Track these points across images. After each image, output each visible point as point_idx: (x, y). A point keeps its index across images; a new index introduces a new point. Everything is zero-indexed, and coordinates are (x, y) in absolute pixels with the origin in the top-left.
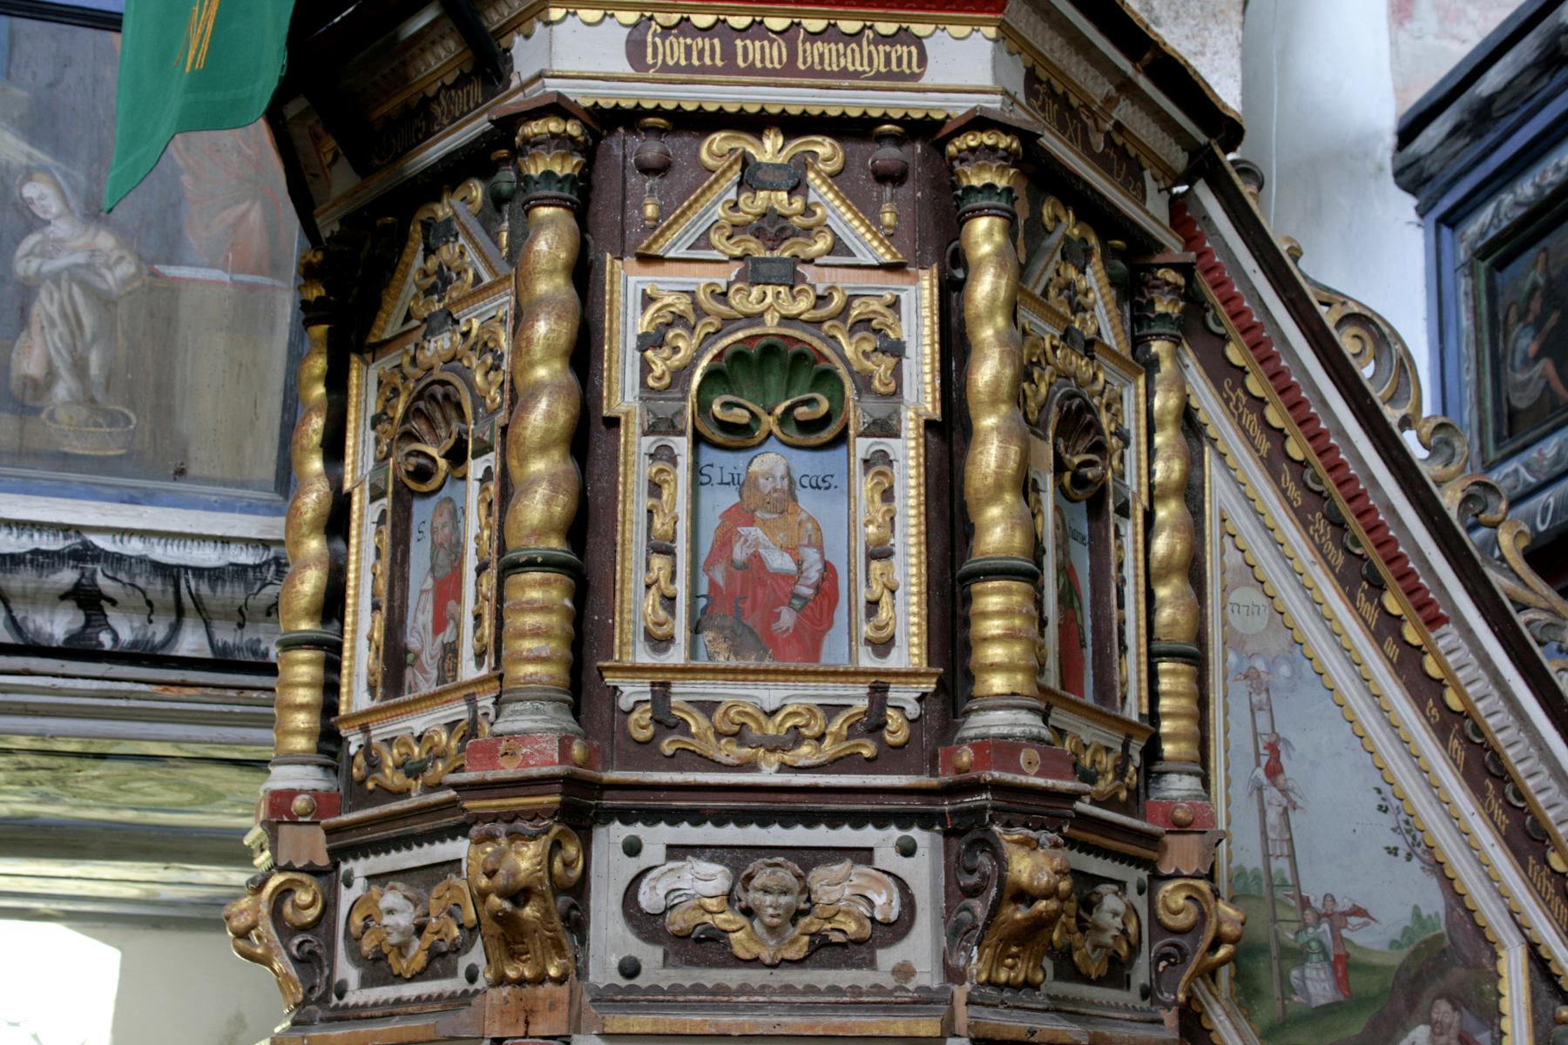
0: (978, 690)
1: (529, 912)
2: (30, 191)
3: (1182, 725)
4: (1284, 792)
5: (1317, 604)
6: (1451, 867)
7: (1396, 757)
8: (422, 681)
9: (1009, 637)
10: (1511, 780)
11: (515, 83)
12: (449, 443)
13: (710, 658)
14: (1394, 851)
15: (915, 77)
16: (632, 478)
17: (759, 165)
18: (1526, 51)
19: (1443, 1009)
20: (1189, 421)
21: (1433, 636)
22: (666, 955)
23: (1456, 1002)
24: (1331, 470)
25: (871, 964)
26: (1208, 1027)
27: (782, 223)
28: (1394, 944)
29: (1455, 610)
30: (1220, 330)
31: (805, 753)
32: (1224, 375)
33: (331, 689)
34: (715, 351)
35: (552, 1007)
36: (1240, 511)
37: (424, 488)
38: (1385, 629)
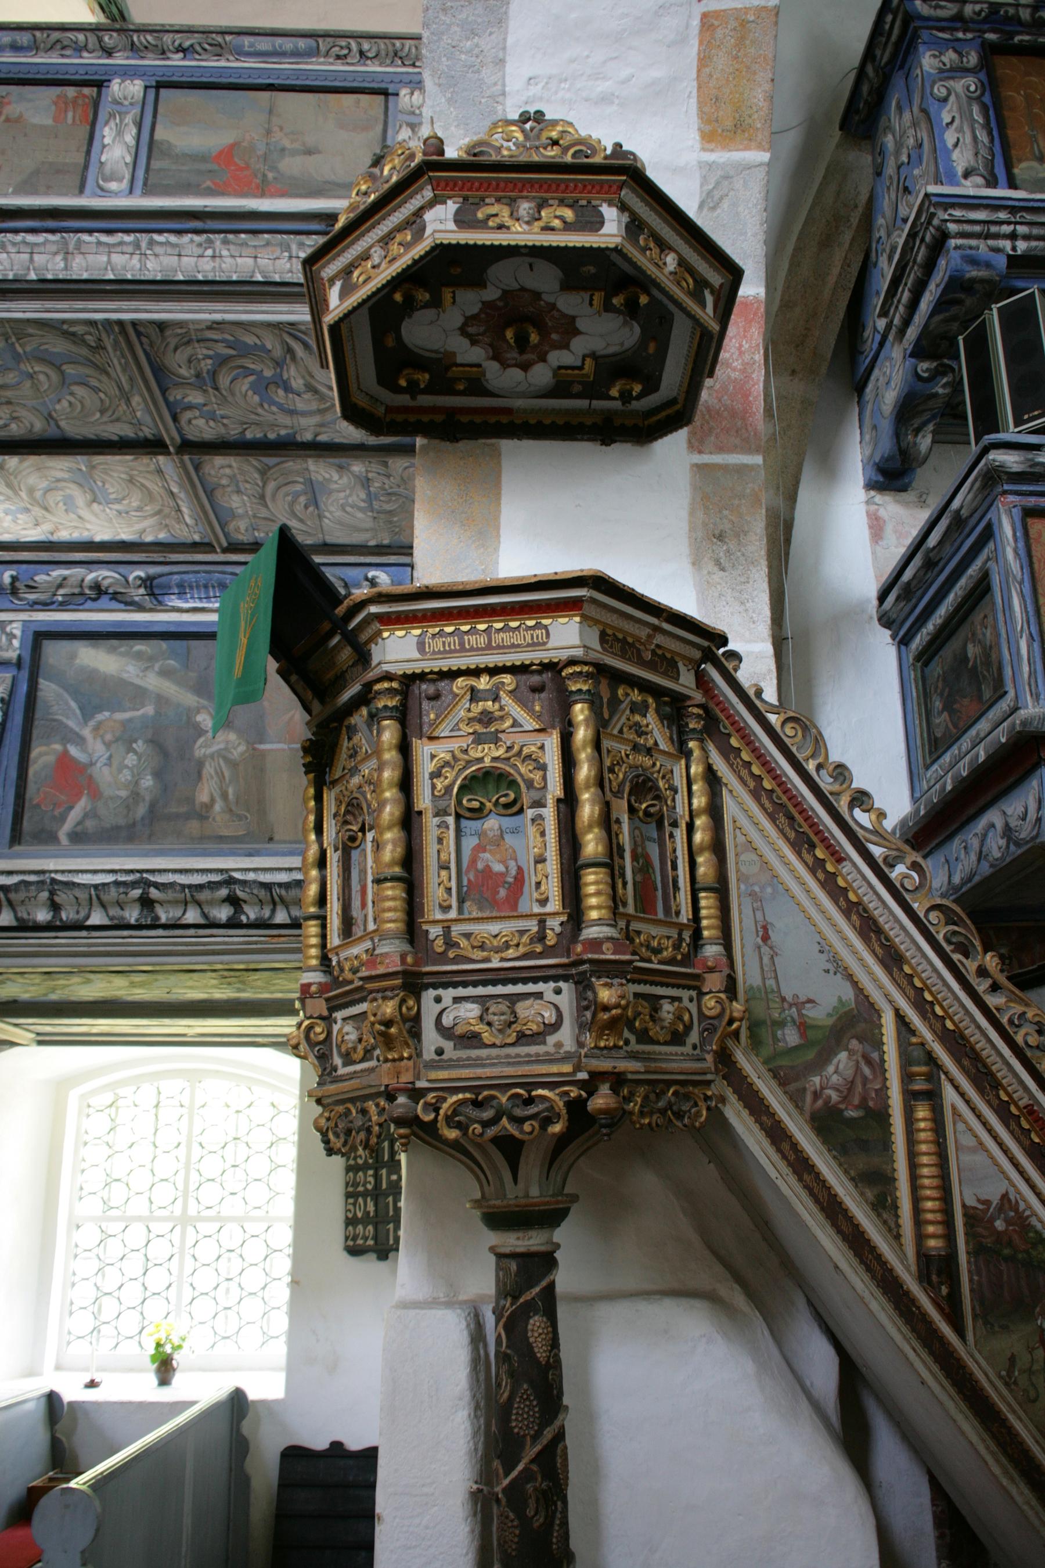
0: (585, 918)
1: (393, 1030)
2: (199, 718)
3: (713, 921)
4: (771, 948)
5: (782, 857)
8: (358, 931)
9: (598, 893)
10: (883, 932)
11: (373, 665)
12: (360, 825)
13: (470, 913)
14: (827, 971)
15: (545, 644)
16: (429, 837)
17: (479, 691)
18: (917, 561)
19: (854, 1044)
20: (711, 777)
22: (455, 1045)
23: (861, 1039)
24: (785, 793)
25: (544, 1043)
27: (490, 716)
28: (829, 1015)
29: (847, 854)
30: (727, 732)
31: (511, 953)
32: (728, 753)
33: (324, 936)
34: (463, 776)
35: (407, 1070)
37: (355, 845)
38: (816, 867)
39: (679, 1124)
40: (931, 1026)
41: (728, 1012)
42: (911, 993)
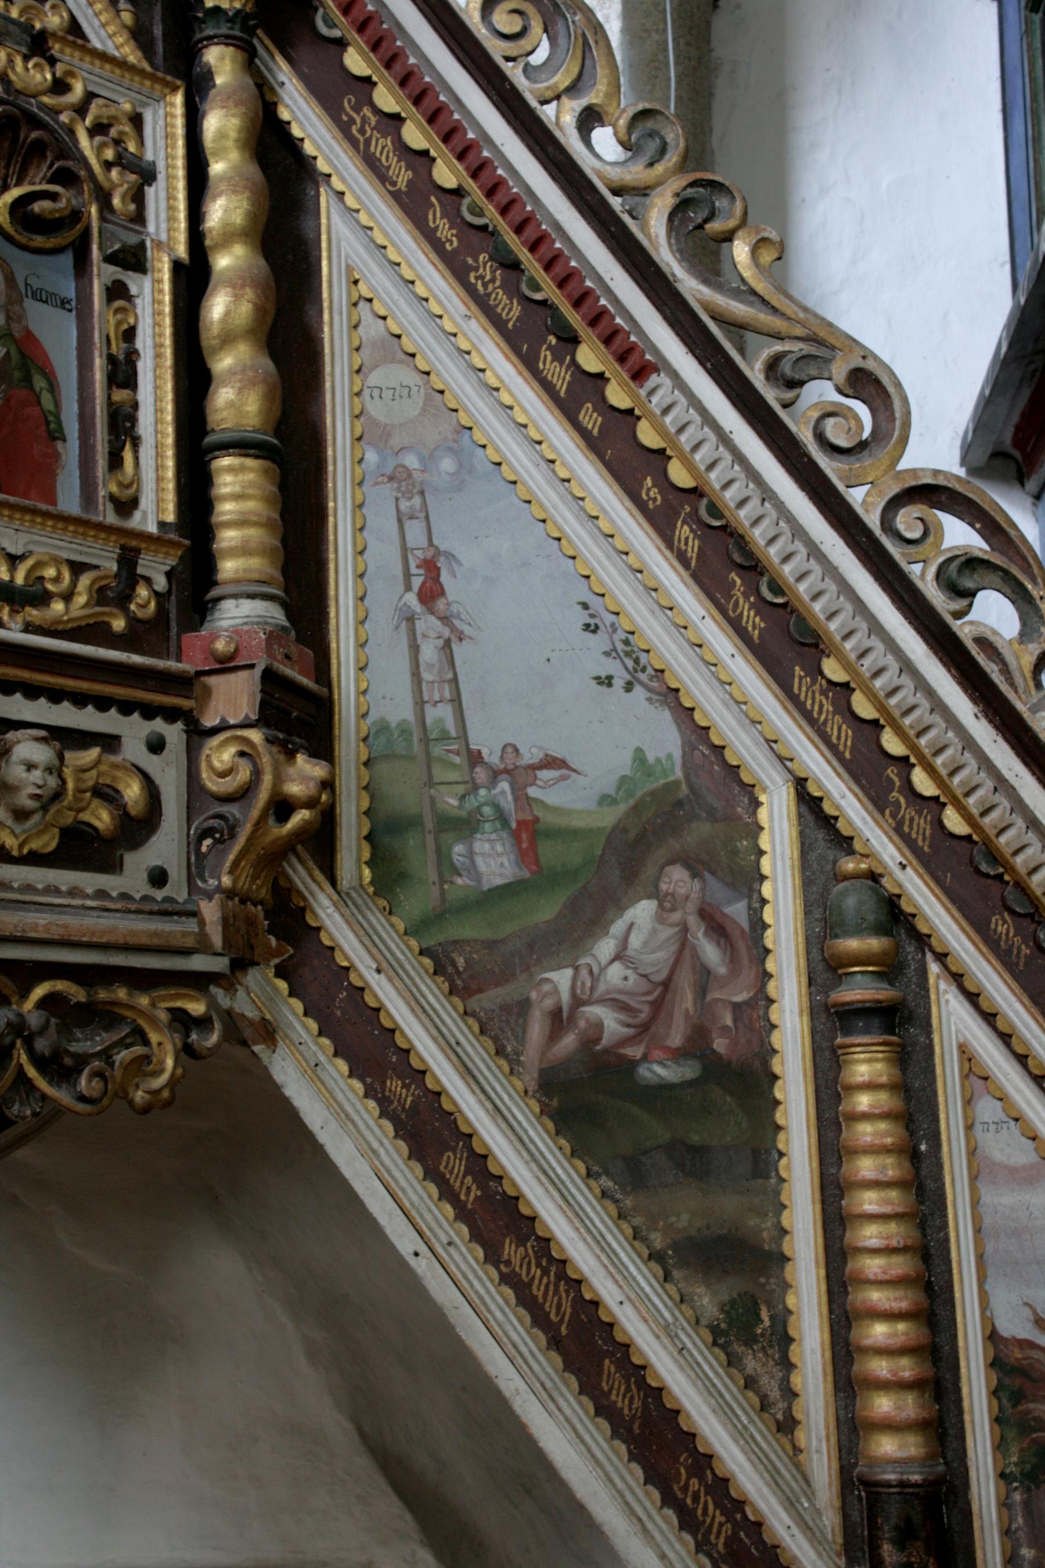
4: (445, 620)
6: (688, 693)
7: (603, 559)
14: (607, 681)
19: (677, 878)
21: (643, 393)
23: (695, 866)
26: (314, 924)
28: (605, 800)
30: (336, 33)
36: (374, 266)
39: (60, 1095)
40: (898, 830)
41: (267, 779)
42: (844, 734)
